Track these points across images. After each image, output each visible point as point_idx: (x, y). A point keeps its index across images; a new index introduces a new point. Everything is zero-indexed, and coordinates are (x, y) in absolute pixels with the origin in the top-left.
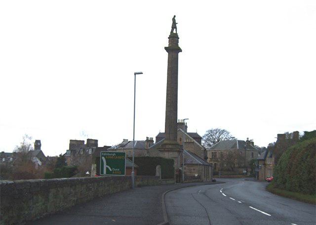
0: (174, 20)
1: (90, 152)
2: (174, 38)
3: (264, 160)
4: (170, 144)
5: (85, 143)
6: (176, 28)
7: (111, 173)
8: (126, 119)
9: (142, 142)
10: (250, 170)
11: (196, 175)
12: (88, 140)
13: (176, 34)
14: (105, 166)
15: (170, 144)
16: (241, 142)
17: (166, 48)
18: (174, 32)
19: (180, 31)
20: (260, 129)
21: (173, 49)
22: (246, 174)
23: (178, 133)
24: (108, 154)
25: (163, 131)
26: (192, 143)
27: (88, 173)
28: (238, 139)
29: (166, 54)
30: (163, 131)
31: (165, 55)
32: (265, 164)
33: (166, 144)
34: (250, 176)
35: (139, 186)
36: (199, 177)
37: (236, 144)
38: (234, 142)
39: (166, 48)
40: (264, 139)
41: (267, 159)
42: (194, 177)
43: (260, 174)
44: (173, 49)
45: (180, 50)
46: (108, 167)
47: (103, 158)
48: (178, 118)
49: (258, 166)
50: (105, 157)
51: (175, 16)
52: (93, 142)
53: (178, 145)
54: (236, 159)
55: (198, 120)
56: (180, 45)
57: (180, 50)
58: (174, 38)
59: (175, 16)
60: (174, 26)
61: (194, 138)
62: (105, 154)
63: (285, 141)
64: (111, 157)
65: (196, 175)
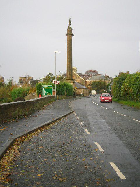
0: (70, 21)
1: (30, 83)
2: (70, 29)
5: (27, 78)
6: (71, 24)
7: (47, 94)
11: (81, 94)
13: (71, 27)
14: (44, 92)
17: (66, 34)
18: (70, 26)
20: (111, 70)
21: (70, 34)
23: (73, 74)
24: (45, 87)
26: (79, 78)
29: (66, 37)
30: (66, 73)
31: (66, 38)
35: (59, 99)
36: (83, 94)
39: (66, 34)
40: (113, 74)
42: (80, 95)
44: (70, 34)
45: (72, 35)
46: (46, 92)
47: (43, 88)
48: (93, 91)
50: (44, 88)
51: (70, 19)
52: (31, 78)
53: (73, 80)
56: (73, 33)
57: (72, 35)
58: (70, 29)
59: (70, 19)
60: (70, 24)
61: (80, 76)
62: (44, 87)
63: (122, 77)
64: (46, 88)
65: (81, 94)
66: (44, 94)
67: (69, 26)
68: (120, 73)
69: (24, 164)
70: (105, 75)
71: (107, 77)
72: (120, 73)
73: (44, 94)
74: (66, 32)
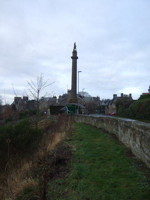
2: (75, 53)
3: (108, 106)
4: (74, 100)
6: (76, 48)
8: (60, 87)
9: (51, 98)
10: (99, 110)
12: (24, 97)
13: (76, 51)
14: (67, 110)
15: (74, 100)
16: (94, 98)
18: (75, 50)
19: (78, 49)
21: (75, 58)
22: (98, 112)
25: (136, 96)
27: (45, 113)
28: (93, 96)
29: (71, 60)
31: (71, 61)
32: (108, 108)
33: (72, 100)
34: (100, 113)
37: (92, 99)
38: (91, 98)
39: (72, 57)
41: (109, 105)
43: (106, 112)
44: (75, 58)
45: (72, 57)
47: (67, 107)
49: (105, 109)
50: (67, 106)
51: (75, 43)
54: (96, 106)
55: (89, 88)
56: (78, 56)
57: (72, 57)
58: (75, 53)
59: (75, 43)
66: (67, 113)
67: (74, 50)
68: (143, 93)
69: (103, 110)
70: (111, 98)
71: (106, 99)
72: (17, 99)
73: (67, 113)
74: (78, 61)
